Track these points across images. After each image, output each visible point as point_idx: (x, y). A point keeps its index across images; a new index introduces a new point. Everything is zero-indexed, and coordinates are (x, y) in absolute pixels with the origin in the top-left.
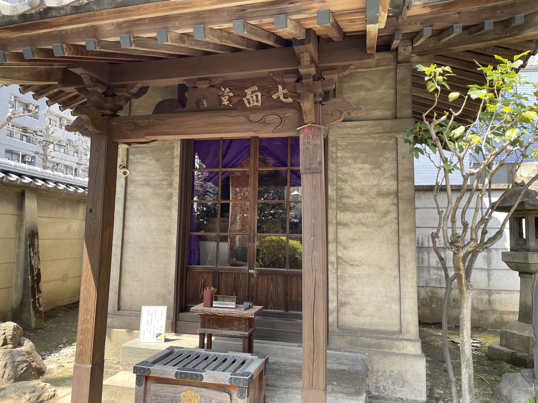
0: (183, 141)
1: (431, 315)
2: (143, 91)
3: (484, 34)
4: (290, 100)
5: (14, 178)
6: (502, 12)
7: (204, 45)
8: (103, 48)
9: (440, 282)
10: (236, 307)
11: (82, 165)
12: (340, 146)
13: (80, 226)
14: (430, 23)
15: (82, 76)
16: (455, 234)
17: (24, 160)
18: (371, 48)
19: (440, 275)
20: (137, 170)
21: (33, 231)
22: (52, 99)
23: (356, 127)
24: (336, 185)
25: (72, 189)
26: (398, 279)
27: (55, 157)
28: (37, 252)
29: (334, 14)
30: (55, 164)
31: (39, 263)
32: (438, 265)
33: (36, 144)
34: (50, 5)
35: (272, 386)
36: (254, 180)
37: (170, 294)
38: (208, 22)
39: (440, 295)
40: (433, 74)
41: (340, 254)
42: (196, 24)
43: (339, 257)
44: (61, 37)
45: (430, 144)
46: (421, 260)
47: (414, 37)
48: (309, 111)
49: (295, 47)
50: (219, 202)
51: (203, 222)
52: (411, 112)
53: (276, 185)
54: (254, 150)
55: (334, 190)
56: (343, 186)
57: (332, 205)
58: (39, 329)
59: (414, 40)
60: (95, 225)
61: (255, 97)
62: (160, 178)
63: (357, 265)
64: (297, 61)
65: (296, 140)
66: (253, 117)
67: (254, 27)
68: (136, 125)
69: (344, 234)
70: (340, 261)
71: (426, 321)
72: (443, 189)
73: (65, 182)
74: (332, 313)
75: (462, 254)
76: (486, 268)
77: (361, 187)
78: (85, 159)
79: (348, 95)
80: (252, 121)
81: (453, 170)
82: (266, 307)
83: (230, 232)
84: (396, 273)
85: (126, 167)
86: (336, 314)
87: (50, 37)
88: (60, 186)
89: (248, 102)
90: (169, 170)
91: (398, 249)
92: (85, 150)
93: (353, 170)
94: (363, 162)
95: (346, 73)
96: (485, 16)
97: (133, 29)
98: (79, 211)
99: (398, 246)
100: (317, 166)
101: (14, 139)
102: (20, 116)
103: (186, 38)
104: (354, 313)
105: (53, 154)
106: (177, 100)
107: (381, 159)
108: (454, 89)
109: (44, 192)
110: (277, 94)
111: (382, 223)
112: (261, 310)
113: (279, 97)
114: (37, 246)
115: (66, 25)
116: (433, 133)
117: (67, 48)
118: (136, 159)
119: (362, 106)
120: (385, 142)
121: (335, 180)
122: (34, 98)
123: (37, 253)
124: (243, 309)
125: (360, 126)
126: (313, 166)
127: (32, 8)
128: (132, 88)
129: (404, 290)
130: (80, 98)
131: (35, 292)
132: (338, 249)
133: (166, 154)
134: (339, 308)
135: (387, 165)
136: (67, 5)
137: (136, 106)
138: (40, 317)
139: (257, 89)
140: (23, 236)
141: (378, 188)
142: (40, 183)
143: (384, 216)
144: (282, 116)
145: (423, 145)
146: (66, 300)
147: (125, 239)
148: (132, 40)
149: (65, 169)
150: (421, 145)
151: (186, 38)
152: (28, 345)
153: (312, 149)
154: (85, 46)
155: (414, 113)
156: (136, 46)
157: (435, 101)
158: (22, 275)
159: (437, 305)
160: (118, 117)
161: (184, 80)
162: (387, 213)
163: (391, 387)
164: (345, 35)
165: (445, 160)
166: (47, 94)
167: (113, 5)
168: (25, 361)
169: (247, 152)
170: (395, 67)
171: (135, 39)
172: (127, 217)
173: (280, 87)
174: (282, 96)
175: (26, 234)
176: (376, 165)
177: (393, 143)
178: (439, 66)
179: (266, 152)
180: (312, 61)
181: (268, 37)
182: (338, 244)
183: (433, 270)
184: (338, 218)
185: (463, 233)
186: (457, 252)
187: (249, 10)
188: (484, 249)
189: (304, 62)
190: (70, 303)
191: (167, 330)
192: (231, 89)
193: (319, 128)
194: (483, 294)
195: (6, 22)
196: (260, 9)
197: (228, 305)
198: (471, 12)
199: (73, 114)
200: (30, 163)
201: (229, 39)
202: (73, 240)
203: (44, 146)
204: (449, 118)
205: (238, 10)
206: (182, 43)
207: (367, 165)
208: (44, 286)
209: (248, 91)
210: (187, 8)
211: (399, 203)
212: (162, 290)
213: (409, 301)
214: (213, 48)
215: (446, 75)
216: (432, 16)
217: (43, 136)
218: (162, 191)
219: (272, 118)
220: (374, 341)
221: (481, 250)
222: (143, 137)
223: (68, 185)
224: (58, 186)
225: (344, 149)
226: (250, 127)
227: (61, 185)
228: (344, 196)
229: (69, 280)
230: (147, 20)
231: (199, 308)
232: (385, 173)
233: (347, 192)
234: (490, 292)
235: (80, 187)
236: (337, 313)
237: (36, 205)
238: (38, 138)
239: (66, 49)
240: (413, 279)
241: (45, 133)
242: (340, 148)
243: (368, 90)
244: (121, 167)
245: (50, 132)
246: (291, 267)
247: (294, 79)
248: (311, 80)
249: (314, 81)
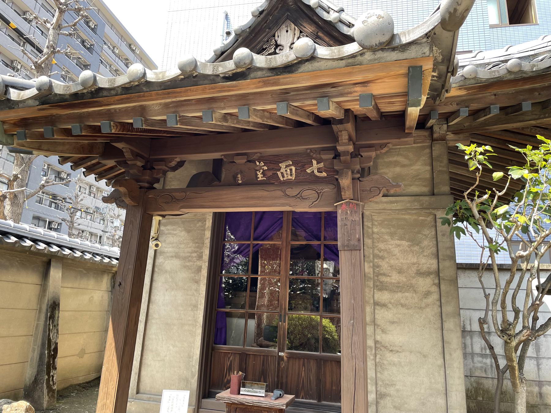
0: (215, 214)
1: (477, 410)
2: (181, 164)
3: (522, 114)
4: (324, 174)
5: (42, 246)
6: (540, 94)
7: (245, 123)
8: (148, 126)
9: (485, 371)
10: (266, 396)
11: (107, 232)
12: (376, 221)
13: (102, 297)
14: (466, 104)
15: (124, 150)
16: (506, 321)
17: (51, 227)
18: (410, 128)
19: (485, 364)
20: (167, 242)
21: (54, 302)
22: (89, 170)
23: (392, 202)
24: (373, 262)
25: (98, 258)
26: (443, 369)
27: (82, 225)
28: (56, 324)
29: (374, 97)
30: (81, 232)
32: (482, 352)
33: (63, 211)
34: (102, 86)
36: (286, 254)
37: (193, 377)
38: (252, 104)
40: (473, 153)
41: (378, 338)
42: (241, 105)
43: (378, 341)
44: (110, 115)
45: (472, 223)
47: (449, 116)
48: (348, 187)
49: (334, 127)
50: (249, 276)
51: (228, 296)
52: (449, 189)
53: (307, 258)
54: (287, 224)
55: (370, 267)
56: (380, 263)
57: (369, 282)
58: (51, 410)
59: (450, 119)
60: (123, 301)
61: (289, 170)
62: (189, 250)
63: (398, 351)
64: (335, 139)
66: (289, 192)
67: (296, 108)
68: (173, 198)
69: (382, 315)
70: (378, 346)
72: (489, 268)
73: (92, 251)
74: (370, 406)
75: (514, 344)
76: (535, 356)
77: (399, 264)
78: (111, 227)
79: (382, 171)
80: (289, 196)
81: (500, 251)
82: (297, 397)
83: (257, 309)
84: (440, 361)
86: (375, 407)
87: (99, 114)
88: (86, 255)
89: (282, 176)
90: (199, 242)
91: (441, 334)
92: (112, 217)
93: (390, 247)
94: (401, 239)
95: (384, 151)
96: (522, 97)
97: (180, 109)
98: (102, 282)
99: (441, 331)
100: (356, 243)
101: (43, 205)
102: (53, 184)
103: (229, 117)
104: (395, 407)
105: (80, 221)
106: (211, 172)
107: (420, 235)
108: (498, 168)
109: (70, 262)
110: (311, 168)
111: (423, 305)
112: (292, 399)
113: (313, 171)
114: (57, 318)
115: (116, 104)
116: (475, 211)
117: (114, 125)
118: (167, 230)
119: (401, 184)
120: (423, 218)
121: (372, 257)
122: (72, 169)
123: (56, 326)
124: (273, 398)
125: (396, 202)
126: (352, 243)
127: (85, 89)
128: (171, 162)
129: (450, 381)
130: (117, 169)
131: (50, 368)
132: (376, 332)
133: (198, 225)
134: (378, 400)
135: (425, 243)
136: (118, 87)
137: (171, 178)
138: (53, 396)
139: (291, 163)
140: (44, 307)
141: (418, 267)
142: (67, 252)
143: (425, 297)
144: (319, 192)
145: (465, 223)
146: (81, 378)
147: (150, 314)
148: (178, 119)
149: (90, 237)
150: (462, 223)
151: (229, 117)
153: (350, 226)
154: (132, 124)
155: (451, 189)
156: (181, 125)
157: (476, 179)
158: (39, 349)
159: (483, 398)
160: (155, 190)
161: (222, 155)
162: (427, 294)
164: (383, 115)
165: (490, 240)
166: (85, 165)
167: (163, 87)
169: (279, 225)
170: (430, 144)
171: (181, 118)
173: (314, 162)
174: (316, 170)
175: (48, 305)
176: (414, 242)
177: (432, 220)
178: (479, 145)
179: (298, 225)
180: (350, 139)
181: (308, 117)
182: (376, 326)
183: (477, 357)
184: (376, 298)
185: (515, 320)
186: (509, 341)
187: (292, 93)
188: (536, 337)
189: (342, 140)
190: (84, 382)
192: (266, 163)
193: (357, 204)
194: (533, 386)
195: (57, 99)
196: (304, 92)
197: (257, 392)
198: (508, 93)
199: (113, 187)
200: (56, 230)
201: (270, 118)
202: (94, 312)
203: (71, 214)
204: (492, 196)
205: (282, 93)
206: (224, 122)
207: (405, 242)
208: (60, 362)
209: (283, 165)
210: (233, 90)
211: (441, 284)
212: (185, 372)
213: (456, 395)
214: (253, 126)
215: (487, 154)
216: (468, 97)
217: (72, 203)
218: (191, 263)
219: (309, 193)
221: (534, 339)
222: (178, 210)
223: (94, 254)
224: (84, 255)
225: (379, 224)
226: (286, 202)
227: (88, 254)
228: (381, 274)
230: (193, 101)
231: (225, 395)
232: (424, 251)
233: (384, 270)
234: (540, 384)
235: (106, 256)
236: (376, 406)
237: (61, 275)
238: (67, 205)
239: (113, 126)
240: (459, 369)
241: (74, 200)
242: (376, 223)
243: (403, 166)
244: (154, 239)
245: (79, 199)
246: (324, 351)
247: (332, 156)
248: (349, 157)
249: (351, 158)
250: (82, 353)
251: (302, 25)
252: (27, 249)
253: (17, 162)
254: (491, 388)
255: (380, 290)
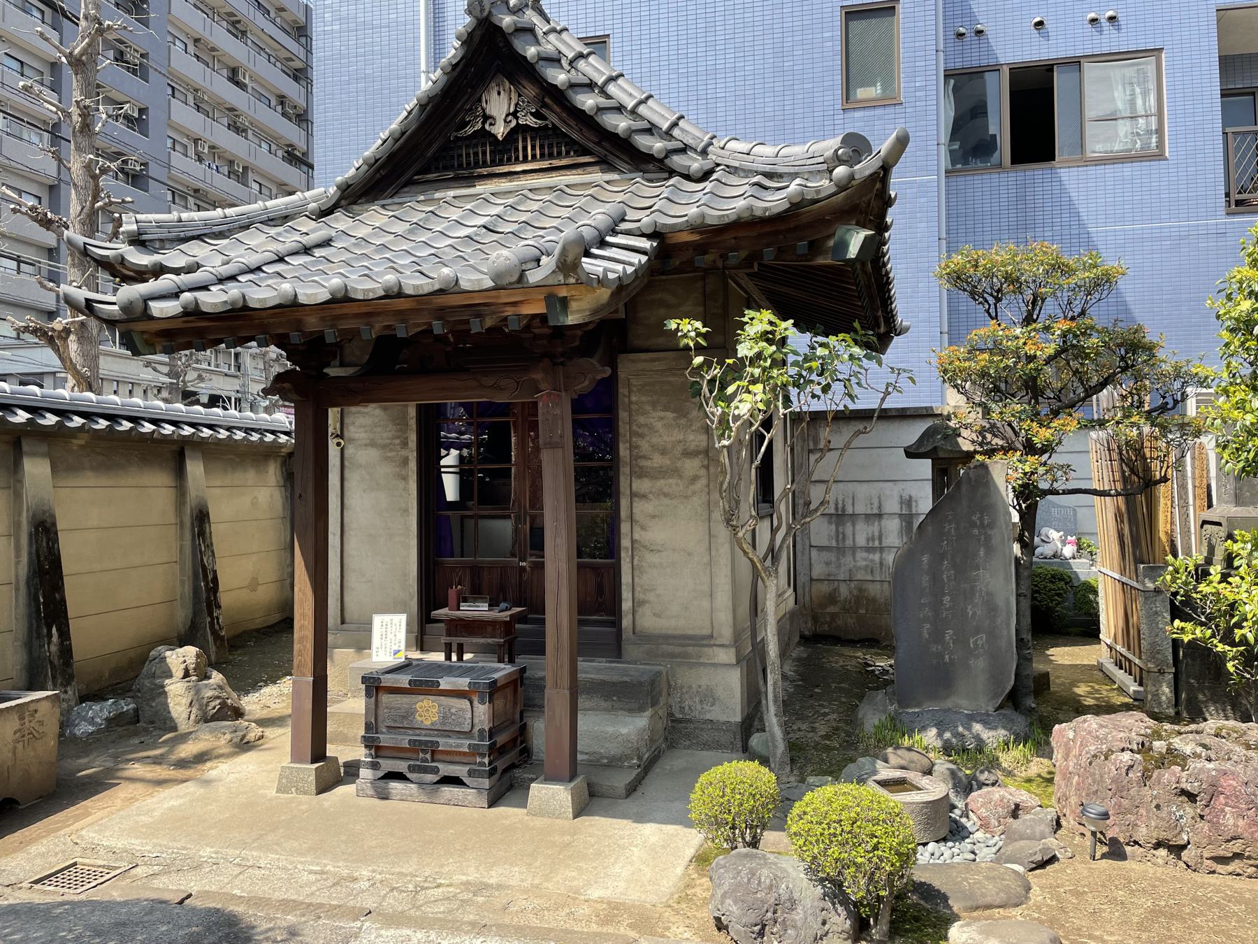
5: (168, 429)
9: (872, 572)
12: (635, 386)
13: (272, 496)
19: (872, 561)
21: (201, 512)
23: (653, 360)
25: (255, 437)
31: (214, 562)
35: (534, 706)
39: (873, 594)
41: (636, 536)
46: (841, 536)
56: (640, 443)
62: (390, 435)
63: (659, 551)
65: (535, 404)
69: (641, 508)
71: (850, 637)
85: (341, 436)
94: (666, 409)
104: (654, 614)
109: (212, 447)
111: (689, 493)
123: (210, 546)
142: (206, 432)
146: (258, 621)
152: (217, 677)
163: (699, 707)
168: (218, 697)
172: (347, 493)
191: (408, 647)
208: (225, 598)
220: (678, 650)
223: (248, 430)
228: (640, 457)
229: (260, 588)
250: (254, 585)
251: (520, 83)
252: (148, 436)
253: (73, 260)
254: (878, 596)
255: (640, 477)
